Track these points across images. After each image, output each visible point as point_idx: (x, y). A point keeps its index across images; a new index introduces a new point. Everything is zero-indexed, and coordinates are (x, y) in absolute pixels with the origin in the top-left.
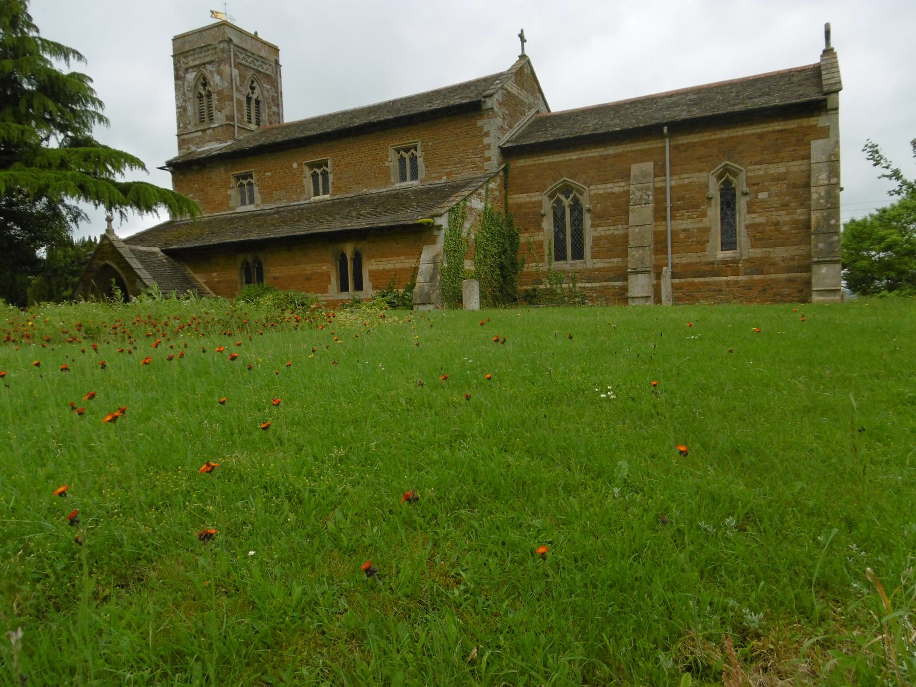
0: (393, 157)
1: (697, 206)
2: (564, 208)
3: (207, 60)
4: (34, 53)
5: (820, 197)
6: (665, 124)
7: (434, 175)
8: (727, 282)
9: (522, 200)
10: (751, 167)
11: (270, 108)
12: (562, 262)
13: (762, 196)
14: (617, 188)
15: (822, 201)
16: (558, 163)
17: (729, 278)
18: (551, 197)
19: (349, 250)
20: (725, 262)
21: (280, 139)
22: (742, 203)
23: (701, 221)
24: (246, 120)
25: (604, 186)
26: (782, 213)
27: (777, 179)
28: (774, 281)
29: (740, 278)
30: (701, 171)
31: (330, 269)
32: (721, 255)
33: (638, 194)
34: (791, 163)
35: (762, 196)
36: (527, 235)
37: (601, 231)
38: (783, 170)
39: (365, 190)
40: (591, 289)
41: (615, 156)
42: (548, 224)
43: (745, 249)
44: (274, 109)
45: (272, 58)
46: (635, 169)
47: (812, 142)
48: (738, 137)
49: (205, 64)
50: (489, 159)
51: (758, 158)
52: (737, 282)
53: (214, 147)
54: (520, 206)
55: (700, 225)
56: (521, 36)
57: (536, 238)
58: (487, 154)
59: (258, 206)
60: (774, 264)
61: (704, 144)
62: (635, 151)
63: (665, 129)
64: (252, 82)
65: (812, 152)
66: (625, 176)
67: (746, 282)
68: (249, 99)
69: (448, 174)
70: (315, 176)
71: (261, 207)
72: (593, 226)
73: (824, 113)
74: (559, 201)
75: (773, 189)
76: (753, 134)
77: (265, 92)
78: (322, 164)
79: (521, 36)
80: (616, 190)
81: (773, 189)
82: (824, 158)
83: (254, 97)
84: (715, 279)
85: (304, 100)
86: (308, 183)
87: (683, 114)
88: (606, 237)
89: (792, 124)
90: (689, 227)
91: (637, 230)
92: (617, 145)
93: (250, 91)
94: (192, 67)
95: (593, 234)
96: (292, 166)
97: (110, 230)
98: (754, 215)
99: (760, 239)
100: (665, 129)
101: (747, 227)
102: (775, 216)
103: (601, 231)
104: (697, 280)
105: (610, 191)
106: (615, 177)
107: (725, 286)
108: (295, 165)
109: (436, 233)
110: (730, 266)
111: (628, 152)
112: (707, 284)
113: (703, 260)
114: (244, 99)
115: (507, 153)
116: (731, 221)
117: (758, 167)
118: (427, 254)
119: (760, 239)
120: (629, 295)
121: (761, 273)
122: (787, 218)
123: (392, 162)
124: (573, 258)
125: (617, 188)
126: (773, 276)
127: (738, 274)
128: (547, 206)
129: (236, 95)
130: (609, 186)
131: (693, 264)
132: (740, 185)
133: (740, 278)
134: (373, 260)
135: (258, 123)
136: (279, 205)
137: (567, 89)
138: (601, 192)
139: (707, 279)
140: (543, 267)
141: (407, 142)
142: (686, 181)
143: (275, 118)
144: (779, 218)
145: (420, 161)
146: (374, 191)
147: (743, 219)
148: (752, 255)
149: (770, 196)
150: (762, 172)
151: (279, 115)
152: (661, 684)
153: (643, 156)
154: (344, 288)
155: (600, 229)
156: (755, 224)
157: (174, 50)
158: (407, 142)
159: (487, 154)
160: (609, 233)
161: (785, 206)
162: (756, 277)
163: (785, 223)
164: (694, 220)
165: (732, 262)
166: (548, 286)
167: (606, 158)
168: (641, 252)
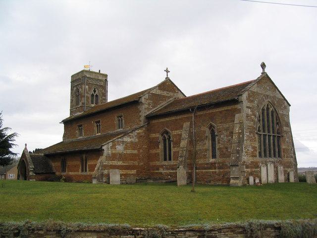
0: (116, 119)
8: (213, 172)
9: (153, 136)
18: (162, 135)
20: (212, 164)
21: (99, 110)
31: (78, 163)
32: (212, 160)
41: (180, 119)
42: (161, 146)
45: (104, 79)
52: (215, 172)
53: (79, 114)
54: (154, 138)
57: (157, 152)
64: (95, 89)
70: (97, 126)
74: (164, 137)
78: (99, 122)
85: (114, 94)
86: (96, 129)
87: (206, 102)
89: (229, 108)
92: (228, 106)
93: (93, 92)
97: (26, 148)
104: (204, 171)
110: (212, 166)
112: (207, 172)
115: (149, 118)
123: (116, 122)
124: (174, 160)
128: (161, 138)
129: (86, 95)
130: (178, 131)
135: (96, 103)
137: (191, 87)
140: (158, 163)
141: (120, 114)
143: (104, 101)
151: (106, 99)
152: (1, 227)
153: (188, 119)
154: (83, 171)
157: (72, 80)
158: (120, 114)
167: (177, 120)
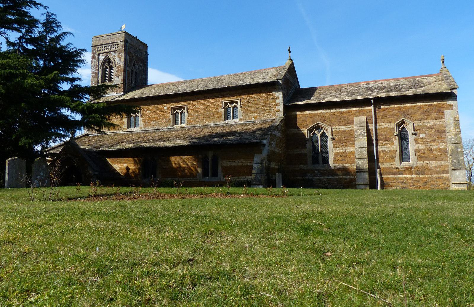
1: (389, 139)
2: (317, 138)
3: (112, 50)
4: (55, 48)
5: (452, 138)
6: (372, 99)
7: (247, 117)
8: (407, 178)
10: (416, 122)
11: (142, 76)
12: (317, 165)
13: (422, 135)
14: (347, 128)
15: (453, 140)
16: (315, 114)
17: (407, 176)
19: (210, 154)
22: (411, 138)
23: (392, 147)
24: (131, 82)
25: (340, 127)
26: (433, 144)
27: (429, 128)
28: (431, 178)
29: (413, 176)
30: (390, 122)
33: (359, 132)
34: (435, 121)
35: (422, 135)
36: (298, 150)
37: (339, 150)
38: (432, 124)
39: (206, 123)
40: (334, 179)
41: (346, 112)
43: (413, 161)
44: (144, 76)
46: (356, 119)
47: (301, 87)
48: (409, 107)
49: (111, 52)
50: (279, 111)
51: (419, 117)
52: (412, 178)
55: (391, 149)
56: (289, 50)
58: (278, 108)
59: (141, 128)
60: (430, 170)
61: (391, 109)
62: (356, 110)
63: (372, 101)
65: (445, 116)
66: (351, 122)
67: (416, 178)
68: (132, 71)
69: (256, 117)
71: (143, 129)
72: (334, 147)
73: (450, 98)
75: (427, 132)
76: (416, 106)
77: (140, 68)
79: (289, 50)
80: (346, 129)
81: (427, 132)
82: (452, 119)
83: (135, 70)
84: (400, 176)
88: (341, 153)
90: (385, 149)
91: (360, 150)
94: (103, 53)
95: (335, 151)
96: (164, 108)
98: (419, 145)
99: (422, 157)
100: (372, 101)
101: (416, 150)
102: (429, 146)
103: (339, 150)
105: (343, 129)
106: (345, 123)
107: (406, 180)
108: (165, 108)
109: (262, 148)
111: (352, 111)
112: (396, 178)
113: (393, 166)
114: (130, 71)
116: (407, 147)
117: (419, 121)
118: (257, 158)
119: (422, 157)
120: (357, 183)
121: (424, 173)
122: (435, 147)
125: (347, 128)
126: (430, 175)
127: (412, 174)
130: (343, 127)
131: (389, 168)
132: (409, 128)
133: (413, 176)
134: (225, 161)
136: (154, 128)
138: (338, 130)
139: (395, 176)
142: (383, 127)
144: (431, 147)
145: (239, 109)
146: (212, 124)
147: (412, 147)
148: (418, 165)
149: (426, 136)
150: (421, 124)
155: (338, 149)
156: (420, 149)
159: (278, 108)
160: (343, 151)
161: (434, 141)
162: (421, 176)
163: (435, 150)
164: (387, 146)
165: (408, 168)
166: (310, 178)
168: (362, 161)
